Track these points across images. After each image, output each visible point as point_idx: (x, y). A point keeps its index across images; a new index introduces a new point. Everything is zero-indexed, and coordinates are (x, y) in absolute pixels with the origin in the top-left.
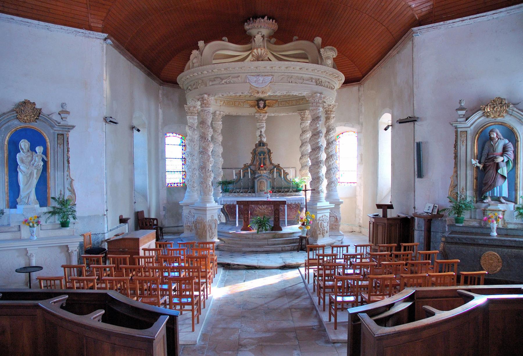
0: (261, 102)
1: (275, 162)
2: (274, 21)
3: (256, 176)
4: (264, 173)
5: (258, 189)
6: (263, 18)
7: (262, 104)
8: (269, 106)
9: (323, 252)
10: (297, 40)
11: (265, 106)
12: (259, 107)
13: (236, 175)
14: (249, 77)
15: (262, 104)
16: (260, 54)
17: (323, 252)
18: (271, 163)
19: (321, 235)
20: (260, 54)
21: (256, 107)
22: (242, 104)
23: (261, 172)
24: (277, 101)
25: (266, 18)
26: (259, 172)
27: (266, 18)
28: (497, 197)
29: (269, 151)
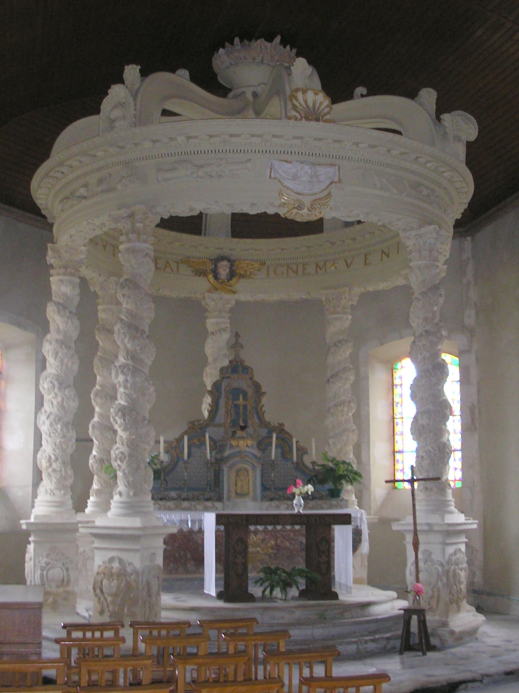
0: (225, 263)
1: (271, 416)
2: (294, 51)
3: (227, 453)
4: (245, 444)
5: (229, 491)
6: (270, 39)
7: (224, 270)
8: (242, 276)
9: (311, 672)
10: (362, 96)
11: (232, 274)
12: (216, 277)
13: (167, 451)
14: (276, 164)
15: (224, 270)
16: (310, 104)
17: (311, 672)
18: (263, 423)
19: (454, 605)
20: (310, 104)
21: (211, 276)
22: (174, 266)
23: (241, 443)
24: (263, 263)
25: (278, 39)
26: (234, 443)
27: (278, 39)
28: (61, 652)
29: (257, 387)
